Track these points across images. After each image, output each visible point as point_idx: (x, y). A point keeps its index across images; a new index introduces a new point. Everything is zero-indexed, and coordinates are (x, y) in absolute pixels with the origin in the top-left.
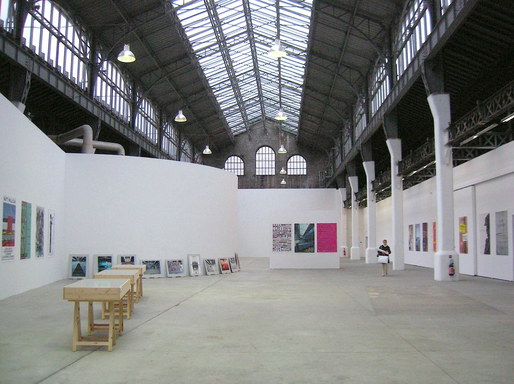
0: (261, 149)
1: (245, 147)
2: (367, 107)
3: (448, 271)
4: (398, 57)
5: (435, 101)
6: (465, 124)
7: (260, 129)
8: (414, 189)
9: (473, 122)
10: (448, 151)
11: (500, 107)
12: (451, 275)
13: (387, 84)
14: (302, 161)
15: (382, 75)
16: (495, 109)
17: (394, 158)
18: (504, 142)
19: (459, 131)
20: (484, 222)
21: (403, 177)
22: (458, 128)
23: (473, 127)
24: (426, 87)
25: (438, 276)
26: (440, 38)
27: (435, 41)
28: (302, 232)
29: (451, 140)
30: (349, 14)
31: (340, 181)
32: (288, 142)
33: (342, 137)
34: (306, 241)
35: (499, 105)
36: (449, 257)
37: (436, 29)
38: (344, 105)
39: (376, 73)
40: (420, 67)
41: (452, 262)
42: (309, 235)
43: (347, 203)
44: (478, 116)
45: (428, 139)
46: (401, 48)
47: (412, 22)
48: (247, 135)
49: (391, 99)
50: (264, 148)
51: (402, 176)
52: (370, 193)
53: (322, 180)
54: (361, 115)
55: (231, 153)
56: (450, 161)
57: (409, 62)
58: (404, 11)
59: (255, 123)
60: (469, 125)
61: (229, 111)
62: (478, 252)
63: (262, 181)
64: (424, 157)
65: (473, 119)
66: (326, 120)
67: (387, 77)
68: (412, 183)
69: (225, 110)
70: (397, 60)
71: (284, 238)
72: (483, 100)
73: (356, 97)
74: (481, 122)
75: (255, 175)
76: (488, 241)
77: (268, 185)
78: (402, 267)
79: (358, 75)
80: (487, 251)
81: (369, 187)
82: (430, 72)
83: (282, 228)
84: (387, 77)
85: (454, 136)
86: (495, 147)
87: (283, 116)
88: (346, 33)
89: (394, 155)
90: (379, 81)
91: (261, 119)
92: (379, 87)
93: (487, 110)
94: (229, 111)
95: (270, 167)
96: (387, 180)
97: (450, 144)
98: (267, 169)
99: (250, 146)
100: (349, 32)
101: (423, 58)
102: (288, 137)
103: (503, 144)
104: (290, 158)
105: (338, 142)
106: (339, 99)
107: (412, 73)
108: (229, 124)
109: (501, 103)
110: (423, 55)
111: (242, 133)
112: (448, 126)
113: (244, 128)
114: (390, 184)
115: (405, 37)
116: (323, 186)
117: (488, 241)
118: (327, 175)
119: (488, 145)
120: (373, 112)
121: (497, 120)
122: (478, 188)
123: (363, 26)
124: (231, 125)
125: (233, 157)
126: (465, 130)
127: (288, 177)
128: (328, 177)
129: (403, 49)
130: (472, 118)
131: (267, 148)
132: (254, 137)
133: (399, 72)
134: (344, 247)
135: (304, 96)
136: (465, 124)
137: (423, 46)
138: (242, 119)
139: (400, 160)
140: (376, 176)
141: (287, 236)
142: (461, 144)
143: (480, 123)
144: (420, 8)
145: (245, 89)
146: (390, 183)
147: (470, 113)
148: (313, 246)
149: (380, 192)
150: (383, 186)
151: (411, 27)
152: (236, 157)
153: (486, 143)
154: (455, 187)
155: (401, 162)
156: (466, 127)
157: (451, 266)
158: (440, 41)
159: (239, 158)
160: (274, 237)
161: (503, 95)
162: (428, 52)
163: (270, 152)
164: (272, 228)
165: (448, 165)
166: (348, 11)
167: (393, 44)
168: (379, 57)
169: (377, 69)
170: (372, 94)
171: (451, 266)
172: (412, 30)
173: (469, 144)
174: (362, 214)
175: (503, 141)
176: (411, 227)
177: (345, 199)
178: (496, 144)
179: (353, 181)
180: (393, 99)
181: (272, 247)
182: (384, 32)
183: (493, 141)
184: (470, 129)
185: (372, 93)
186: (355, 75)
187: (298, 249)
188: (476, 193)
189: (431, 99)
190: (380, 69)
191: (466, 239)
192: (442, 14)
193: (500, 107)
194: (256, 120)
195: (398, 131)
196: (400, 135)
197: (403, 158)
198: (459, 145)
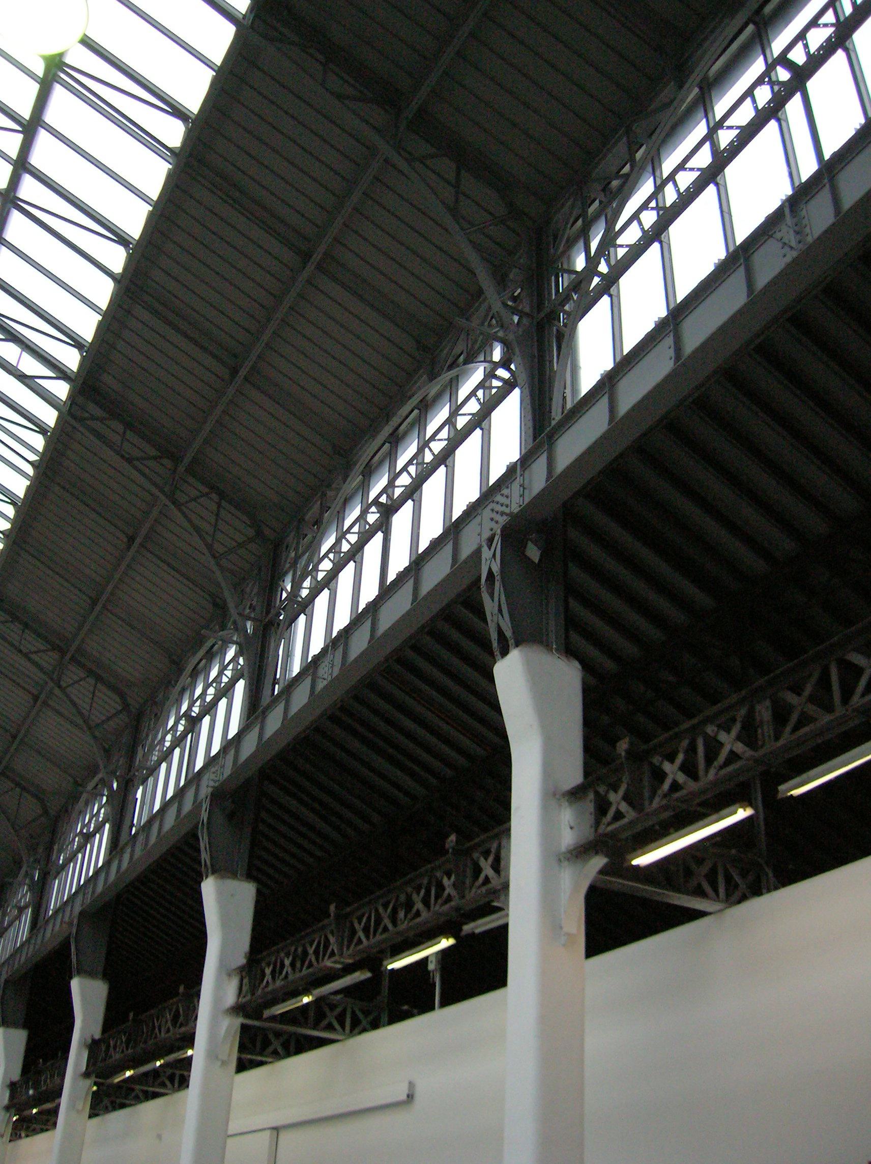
2: (41, 891)
4: (144, 781)
5: (220, 893)
6: (287, 962)
8: (117, 1119)
10: (231, 1025)
11: (390, 926)
13: (103, 839)
15: (94, 819)
16: (324, 955)
17: (83, 1029)
18: (368, 1026)
19: (268, 977)
21: (95, 1084)
22: (268, 971)
23: (384, 936)
24: (205, 856)
26: (265, 739)
27: (249, 747)
29: (244, 1000)
30: (55, 655)
35: (387, 922)
37: (256, 718)
39: (82, 813)
40: (197, 806)
44: (326, 947)
45: (181, 989)
46: (157, 760)
47: (198, 703)
49: (133, 851)
51: (93, 1079)
54: (21, 910)
57: (170, 794)
58: (185, 679)
60: (298, 965)
65: (311, 951)
67: (107, 826)
68: (112, 1102)
70: (141, 788)
73: (18, 863)
74: (333, 959)
84: (107, 826)
86: (344, 1037)
88: (36, 698)
89: (84, 1021)
90: (85, 831)
92: (82, 848)
93: (354, 932)
96: (50, 1086)
97: (238, 1009)
100: (43, 696)
101: (212, 784)
103: (364, 1030)
107: (174, 817)
109: (394, 920)
110: (213, 776)
112: (242, 961)
114: (60, 1095)
115: (174, 736)
119: (330, 1027)
120: (52, 907)
121: (374, 962)
126: (286, 977)
129: (173, 750)
130: (308, 949)
133: (139, 816)
136: (287, 962)
137: (210, 762)
139: (97, 1036)
140: (26, 1070)
142: (267, 1013)
143: (328, 963)
144: (194, 709)
146: (57, 1093)
147: (307, 934)
149: (26, 1113)
150: (37, 1101)
151: (194, 714)
153: (325, 1023)
154: (232, 1130)
155: (99, 1040)
156: (290, 970)
158: (262, 745)
161: (403, 898)
162: (228, 772)
165: (224, 1063)
166: (55, 647)
167: (140, 748)
168: (100, 776)
169: (79, 815)
170: (61, 862)
172: (193, 723)
173: (286, 1018)
175: (364, 1023)
178: (176, 1085)
180: (112, 877)
183: (341, 1020)
184: (298, 975)
185: (62, 858)
186: (30, 808)
188: (278, 1153)
189: (209, 888)
190: (94, 806)
192: (309, 661)
193: (390, 926)
196: (110, 974)
197: (104, 1031)
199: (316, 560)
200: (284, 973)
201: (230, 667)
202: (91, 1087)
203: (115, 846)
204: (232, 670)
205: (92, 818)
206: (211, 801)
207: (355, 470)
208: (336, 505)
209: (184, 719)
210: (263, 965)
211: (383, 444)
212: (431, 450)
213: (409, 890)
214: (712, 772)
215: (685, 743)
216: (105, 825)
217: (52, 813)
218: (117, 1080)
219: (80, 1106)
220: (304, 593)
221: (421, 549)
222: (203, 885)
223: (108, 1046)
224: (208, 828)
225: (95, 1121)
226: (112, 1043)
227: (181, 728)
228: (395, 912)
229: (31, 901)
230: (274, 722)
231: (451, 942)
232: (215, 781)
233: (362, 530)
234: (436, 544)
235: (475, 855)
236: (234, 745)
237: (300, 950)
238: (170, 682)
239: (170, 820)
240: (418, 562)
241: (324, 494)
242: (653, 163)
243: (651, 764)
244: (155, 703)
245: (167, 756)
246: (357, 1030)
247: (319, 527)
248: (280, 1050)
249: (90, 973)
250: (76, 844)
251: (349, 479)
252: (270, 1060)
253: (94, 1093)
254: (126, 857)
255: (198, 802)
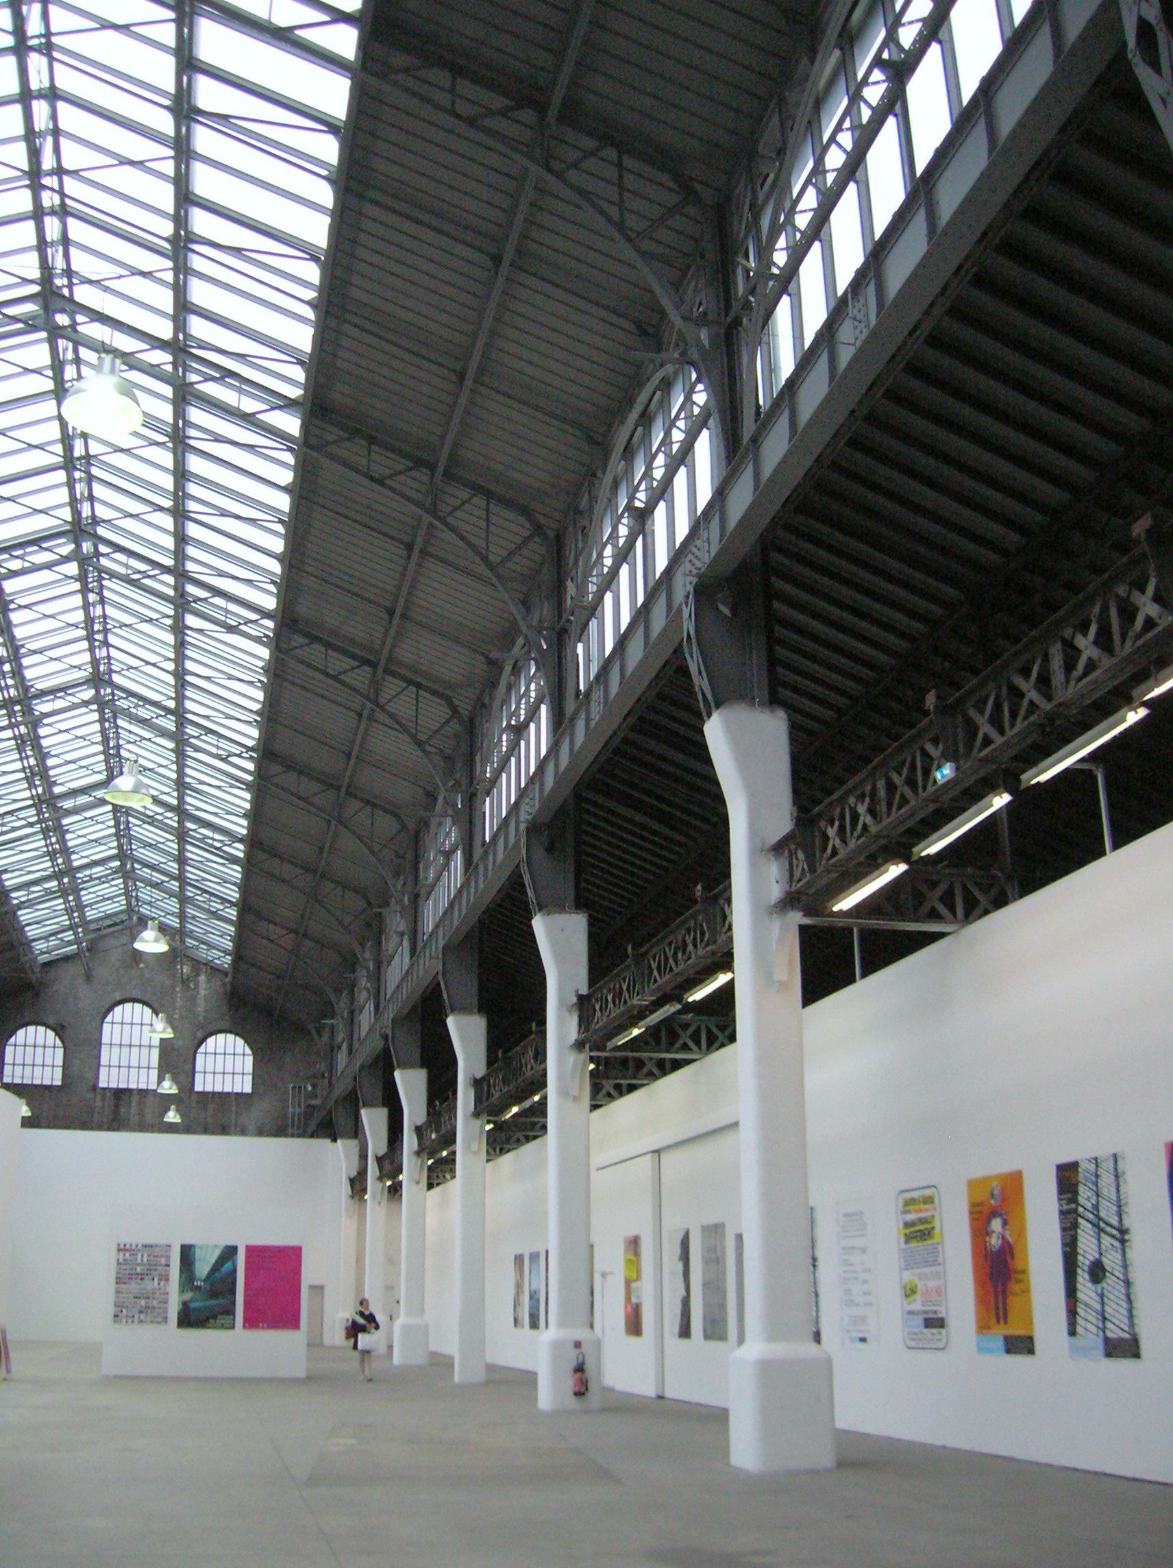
0: (118, 1010)
1: (71, 999)
2: (470, 820)
3: (569, 1383)
5: (549, 930)
7: (120, 950)
9: (625, 994)
12: (579, 1394)
14: (239, 1050)
15: (523, 701)
17: (465, 1072)
18: (726, 1041)
20: (677, 1250)
21: (592, 1059)
24: (701, 683)
25: (545, 1398)
28: (203, 1269)
31: (342, 1119)
32: (202, 992)
33: (353, 991)
34: (213, 1294)
36: (572, 1345)
38: (358, 903)
39: (506, 701)
40: (674, 617)
41: (581, 1357)
42: (222, 1280)
43: (357, 1186)
48: (79, 963)
50: (128, 1006)
51: (485, 1117)
52: (409, 1161)
53: (298, 1110)
54: (448, 855)
55: (28, 1016)
56: (581, 1088)
58: (616, 465)
59: (105, 932)
61: (26, 893)
62: (666, 1335)
63: (117, 1107)
64: (529, 1073)
66: (312, 939)
67: (543, 708)
69: (19, 888)
71: (149, 1285)
72: (641, 945)
73: (431, 796)
75: (95, 1087)
76: (686, 1302)
77: (134, 1119)
78: (480, 1376)
79: (395, 826)
80: (685, 1332)
81: (409, 1141)
82: (539, 853)
83: (145, 1256)
84: (543, 708)
85: (587, 1030)
87: (156, 940)
91: (123, 922)
92: (514, 747)
94: (26, 893)
95: (144, 1063)
98: (134, 1072)
99: (86, 996)
102: (202, 978)
104: (204, 1040)
105: (342, 1004)
106: (345, 886)
108: (27, 929)
111: (67, 958)
113: (69, 943)
114: (455, 1142)
115: (668, 455)
116: (298, 1128)
117: (686, 1302)
118: (314, 1095)
119: (934, 916)
122: (667, 1159)
123: (403, 703)
124: (31, 932)
125: (31, 1029)
127: (194, 1097)
128: (317, 1102)
129: (587, 624)
131: (138, 1006)
132: (101, 972)
134: (952, 1322)
135: (249, 865)
138: (66, 917)
139: (584, 991)
141: (156, 1280)
142: (610, 1045)
143: (636, 1001)
145: (81, 833)
148: (230, 1311)
149: (438, 1156)
151: (638, 504)
152: (41, 1029)
153: (678, 1044)
156: (837, 842)
157: (580, 1369)
158: (762, 491)
159: (51, 1034)
160: (119, 1281)
163: (147, 1020)
164: (112, 1256)
167: (569, 583)
171: (580, 1369)
172: (642, 518)
174: (393, 1219)
176: (519, 1259)
177: (354, 1173)
178: (960, 910)
179: (373, 1120)
180: (614, 689)
181: (111, 1310)
182: (455, 726)
183: (696, 1038)
187: (188, 1319)
191: (638, 1297)
194: (108, 922)
195: (480, 991)
197: (592, 981)
198: (603, 1049)
199: (787, 205)
200: (860, 826)
201: (643, 487)
202: (585, 1066)
203: (559, 722)
204: (646, 490)
205: (521, 700)
206: (697, 601)
207: (824, 42)
208: (803, 115)
209: (626, 515)
210: (722, 901)
211: (636, 429)
212: (866, 102)
213: (1122, 590)
214: (1129, 643)
215: (1097, 610)
216: (539, 707)
217: (466, 714)
218: (508, 1117)
219: (475, 1146)
220: (780, 258)
221: (878, 232)
222: (533, 922)
223: (489, 1086)
224: (528, 864)
225: (490, 1163)
226: (492, 1081)
227: (623, 531)
228: (675, 954)
229: (459, 839)
230: (776, 447)
231: (902, 868)
232: (529, 814)
233: (791, 244)
234: (901, 219)
235: (822, 824)
236: (642, 619)
237: (617, 986)
238: (594, 475)
239: (635, 652)
240: (878, 253)
241: (782, 101)
242: (884, 7)
243: (1117, 596)
244: (578, 512)
245: (610, 581)
246: (714, 1047)
247: (784, 156)
248: (613, 1092)
249: (465, 1010)
250: (504, 744)
251: (819, 56)
252: (645, 1082)
253: (591, 1072)
254: (580, 726)
255: (1066, 50)
